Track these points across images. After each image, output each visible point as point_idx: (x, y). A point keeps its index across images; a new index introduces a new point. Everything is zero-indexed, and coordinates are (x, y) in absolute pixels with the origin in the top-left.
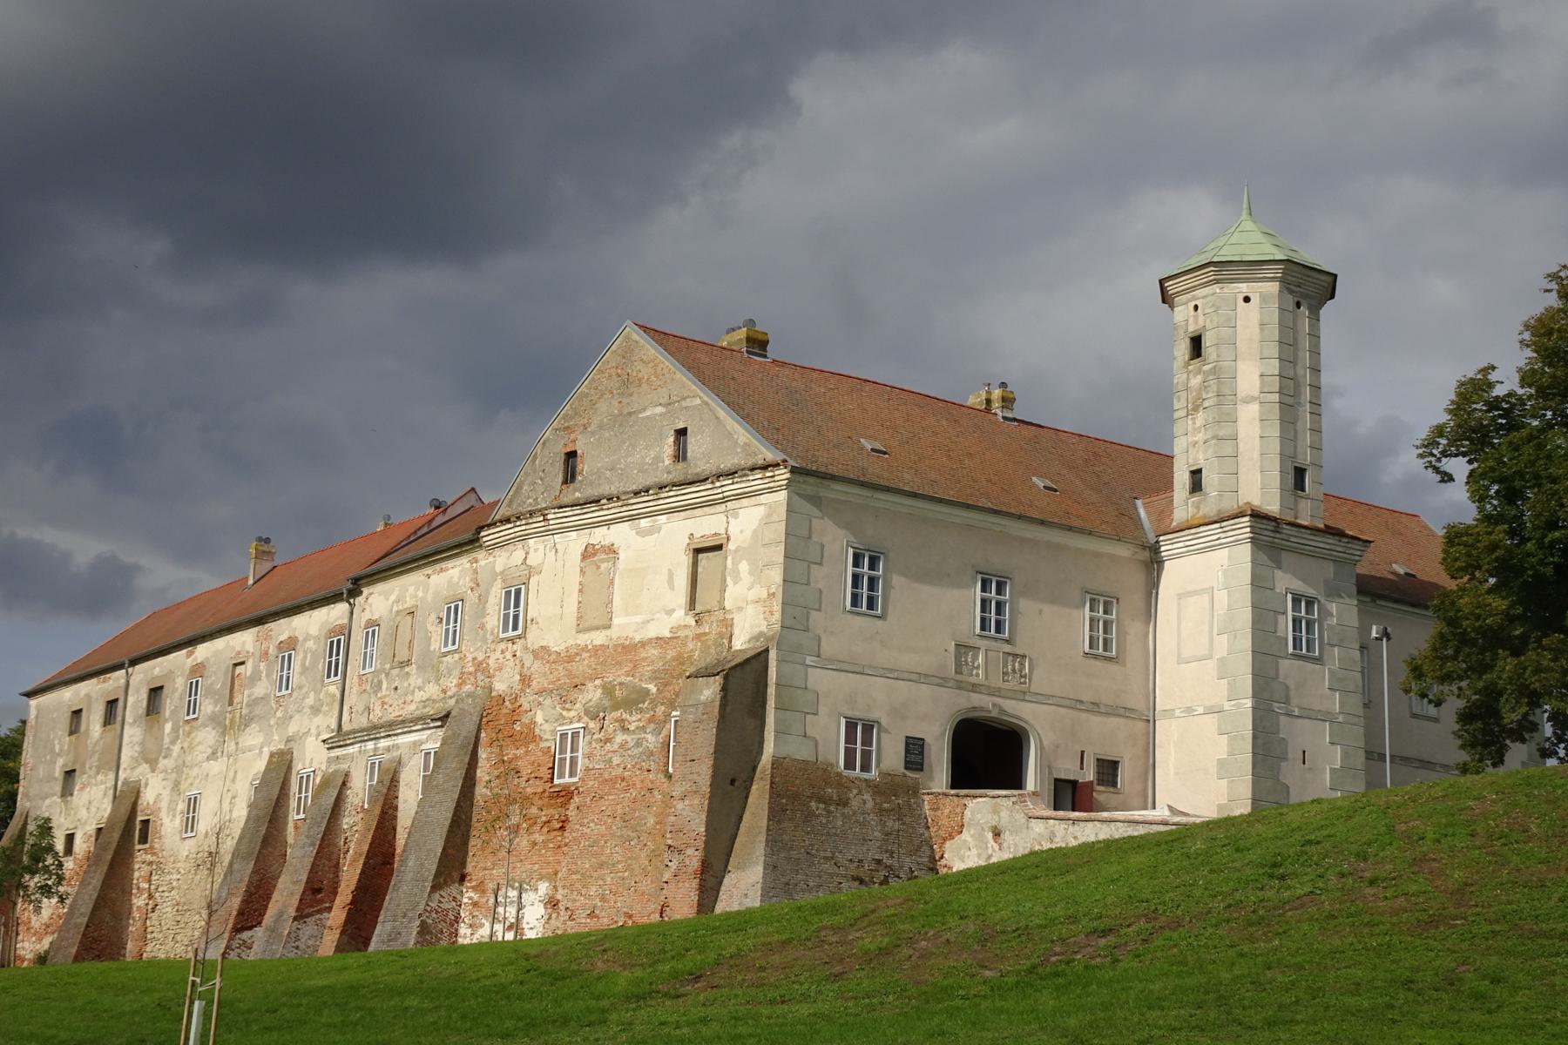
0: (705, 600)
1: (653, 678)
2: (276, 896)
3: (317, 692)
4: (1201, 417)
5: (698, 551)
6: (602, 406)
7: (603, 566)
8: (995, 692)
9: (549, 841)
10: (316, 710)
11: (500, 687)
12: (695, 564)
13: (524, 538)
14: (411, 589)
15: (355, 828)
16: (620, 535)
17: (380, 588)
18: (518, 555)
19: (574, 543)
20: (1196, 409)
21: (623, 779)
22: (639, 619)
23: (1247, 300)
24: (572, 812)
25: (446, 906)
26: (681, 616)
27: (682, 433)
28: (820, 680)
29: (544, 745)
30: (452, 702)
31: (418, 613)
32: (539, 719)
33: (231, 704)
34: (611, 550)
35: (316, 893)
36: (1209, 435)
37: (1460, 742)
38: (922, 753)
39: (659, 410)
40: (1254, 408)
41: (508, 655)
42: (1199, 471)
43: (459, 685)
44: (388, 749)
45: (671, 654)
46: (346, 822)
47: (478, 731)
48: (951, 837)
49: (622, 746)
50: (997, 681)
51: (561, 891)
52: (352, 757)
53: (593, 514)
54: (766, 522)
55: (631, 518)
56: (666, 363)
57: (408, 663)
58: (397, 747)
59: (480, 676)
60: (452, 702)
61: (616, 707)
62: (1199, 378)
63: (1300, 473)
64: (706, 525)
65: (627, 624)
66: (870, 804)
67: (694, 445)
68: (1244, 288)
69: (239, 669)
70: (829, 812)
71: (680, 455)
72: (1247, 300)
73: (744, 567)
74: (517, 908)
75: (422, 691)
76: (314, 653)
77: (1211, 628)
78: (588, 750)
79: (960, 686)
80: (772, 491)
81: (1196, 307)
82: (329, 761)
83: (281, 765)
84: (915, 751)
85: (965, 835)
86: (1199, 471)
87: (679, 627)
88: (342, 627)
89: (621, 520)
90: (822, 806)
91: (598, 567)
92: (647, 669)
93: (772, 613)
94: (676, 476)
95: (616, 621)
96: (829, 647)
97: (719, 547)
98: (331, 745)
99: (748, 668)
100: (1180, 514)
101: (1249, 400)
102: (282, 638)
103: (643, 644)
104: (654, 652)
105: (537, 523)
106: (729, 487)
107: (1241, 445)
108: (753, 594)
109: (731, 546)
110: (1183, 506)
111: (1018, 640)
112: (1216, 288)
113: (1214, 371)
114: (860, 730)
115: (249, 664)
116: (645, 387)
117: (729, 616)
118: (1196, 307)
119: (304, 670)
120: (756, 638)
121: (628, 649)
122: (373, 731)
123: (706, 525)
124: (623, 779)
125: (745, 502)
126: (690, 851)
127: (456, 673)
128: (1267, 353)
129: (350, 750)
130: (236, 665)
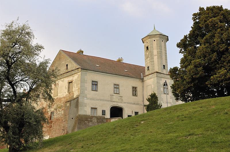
0: (71, 91)
5: (69, 83)
12: (69, 85)
23: (154, 41)
27: (67, 65)
28: (86, 101)
37: (186, 35)
38: (105, 112)
39: (64, 62)
40: (156, 56)
42: (149, 67)
49: (59, 114)
50: (117, 100)
54: (78, 77)
56: (67, 57)
63: (147, 47)
64: (70, 79)
68: (154, 39)
71: (67, 69)
72: (154, 41)
73: (75, 84)
79: (111, 101)
84: (104, 112)
86: (149, 67)
92: (62, 102)
94: (66, 72)
95: (58, 95)
96: (88, 96)
97: (72, 82)
99: (75, 100)
100: (146, 74)
101: (155, 56)
104: (63, 99)
106: (73, 72)
107: (155, 62)
108: (76, 89)
109: (73, 82)
110: (147, 73)
111: (120, 93)
112: (150, 39)
114: (94, 109)
120: (77, 96)
128: (158, 48)
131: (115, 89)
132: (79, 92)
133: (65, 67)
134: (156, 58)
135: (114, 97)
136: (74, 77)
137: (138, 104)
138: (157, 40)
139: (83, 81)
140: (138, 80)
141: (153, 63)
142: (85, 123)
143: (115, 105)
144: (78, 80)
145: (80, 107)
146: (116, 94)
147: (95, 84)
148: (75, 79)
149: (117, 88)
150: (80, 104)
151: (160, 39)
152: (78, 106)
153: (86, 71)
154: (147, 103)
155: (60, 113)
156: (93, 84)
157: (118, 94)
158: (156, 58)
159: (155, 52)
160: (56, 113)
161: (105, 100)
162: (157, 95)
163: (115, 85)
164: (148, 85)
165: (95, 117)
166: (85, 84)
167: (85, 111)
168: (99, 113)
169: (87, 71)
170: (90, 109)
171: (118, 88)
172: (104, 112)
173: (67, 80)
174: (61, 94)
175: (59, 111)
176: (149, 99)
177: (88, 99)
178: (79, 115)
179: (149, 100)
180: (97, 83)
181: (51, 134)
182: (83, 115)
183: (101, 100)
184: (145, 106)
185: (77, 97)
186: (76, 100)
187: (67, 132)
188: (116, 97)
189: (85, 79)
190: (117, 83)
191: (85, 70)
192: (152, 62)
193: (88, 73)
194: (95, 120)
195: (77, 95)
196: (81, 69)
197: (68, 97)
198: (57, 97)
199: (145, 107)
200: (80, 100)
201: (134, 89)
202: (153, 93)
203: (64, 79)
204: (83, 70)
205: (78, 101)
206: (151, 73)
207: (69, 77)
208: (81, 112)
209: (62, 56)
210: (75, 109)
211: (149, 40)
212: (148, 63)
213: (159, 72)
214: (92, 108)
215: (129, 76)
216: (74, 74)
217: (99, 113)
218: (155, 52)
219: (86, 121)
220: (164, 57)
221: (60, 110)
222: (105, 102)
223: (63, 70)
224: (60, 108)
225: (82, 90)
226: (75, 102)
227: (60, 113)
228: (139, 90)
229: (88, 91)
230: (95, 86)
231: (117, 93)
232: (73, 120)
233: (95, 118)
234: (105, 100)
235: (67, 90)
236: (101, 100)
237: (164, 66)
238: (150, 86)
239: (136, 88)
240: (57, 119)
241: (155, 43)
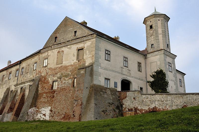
0: (80, 58)
1: (70, 71)
2: (5, 109)
3: (14, 79)
4: (153, 37)
5: (79, 50)
6: (62, 29)
7: (61, 54)
8: (126, 75)
9: (51, 100)
10: (14, 81)
11: (43, 75)
12: (78, 52)
13: (47, 51)
14: (29, 62)
15: (18, 98)
16: (63, 49)
17: (24, 62)
18: (46, 54)
19: (56, 51)
20: (152, 36)
21: (65, 89)
22: (67, 62)
23: (159, 20)
24: (55, 95)
25: (32, 111)
26: (75, 61)
28: (100, 70)
29: (50, 83)
30: (34, 78)
31: (30, 65)
32: (49, 79)
33: (2, 81)
34: (63, 51)
35: (11, 109)
36: (155, 39)
39: (72, 29)
40: (161, 35)
41: (44, 69)
43: (36, 75)
44: (24, 86)
45: (73, 67)
46: (17, 98)
47: (39, 82)
48: (124, 99)
49: (64, 83)
50: (126, 73)
51: (53, 109)
52: (18, 88)
53: (60, 46)
54: (92, 44)
55: (66, 46)
57: (28, 73)
58: (25, 85)
59: (39, 73)
60: (34, 78)
61: (63, 77)
62: (152, 31)
64: (80, 46)
65: (65, 63)
66: (110, 93)
67: (77, 33)
68: (158, 18)
69: (4, 77)
70: (104, 94)
71: (75, 36)
72: (159, 20)
73: (87, 52)
74: (45, 113)
75: (30, 76)
76: (14, 73)
77: (157, 67)
78: (58, 84)
79: (122, 74)
80: (93, 39)
81: (151, 22)
82: (15, 88)
83: (8, 89)
84: (116, 84)
85: (127, 98)
87: (75, 63)
88: (18, 69)
89: (65, 46)
90: (102, 93)
91: (60, 54)
92: (69, 70)
93: (93, 59)
95: (63, 63)
96: (102, 65)
97: (83, 49)
98: (15, 86)
101: (160, 34)
102: (10, 71)
103: (68, 66)
104: (70, 67)
105: (50, 48)
106: (85, 39)
108: (89, 56)
109: (85, 49)
112: (154, 18)
113: (155, 30)
115: (5, 76)
116: (69, 25)
117: (84, 60)
118: (151, 22)
119: (13, 76)
120: (90, 63)
121: (66, 67)
122: (22, 83)
123: (80, 46)
124: (65, 89)
125: (87, 41)
126: (79, 101)
127: (35, 73)
129: (18, 86)
130: (3, 76)
132: (94, 60)
133: (73, 34)
134: (160, 37)
135: (124, 70)
136: (86, 44)
139: (97, 48)
142: (101, 94)
143: (125, 78)
144: (92, 46)
145: (94, 76)
147: (108, 53)
148: (88, 46)
150: (95, 73)
152: (92, 75)
154: (152, 80)
155: (66, 82)
156: (106, 53)
157: (127, 67)
158: (160, 37)
159: (160, 31)
160: (60, 82)
162: (164, 72)
163: (124, 57)
164: (152, 62)
165: (109, 88)
167: (100, 81)
169: (102, 38)
170: (104, 79)
172: (116, 84)
173: (74, 48)
174: (67, 62)
175: (65, 80)
176: (153, 75)
177: (102, 68)
178: (95, 85)
179: (153, 76)
180: (110, 53)
181: (53, 105)
182: (98, 85)
183: (113, 71)
184: (148, 82)
185: (91, 64)
186: (90, 67)
187: (82, 103)
188: (125, 70)
189: (100, 47)
190: (126, 56)
191: (99, 37)
192: (157, 39)
194: (109, 92)
195: (90, 62)
196: (97, 35)
197: (77, 65)
198: (61, 65)
199: (148, 83)
200: (95, 68)
201: (139, 64)
202: (159, 70)
203: (72, 45)
205: (92, 70)
206: (156, 50)
207: (79, 44)
208: (96, 82)
209: (69, 23)
210: (89, 77)
211: (153, 20)
212: (152, 41)
214: (106, 79)
216: (86, 40)
218: (160, 31)
219: (101, 92)
220: (167, 36)
221: (65, 78)
222: (117, 74)
223: (70, 36)
224: (66, 76)
225: (97, 57)
226: (90, 69)
227: (66, 82)
228: (143, 65)
229: (102, 60)
232: (88, 90)
233: (109, 90)
234: (117, 72)
235: (75, 58)
237: (168, 45)
238: (156, 63)
239: (140, 63)
240: (63, 89)
241: (159, 23)
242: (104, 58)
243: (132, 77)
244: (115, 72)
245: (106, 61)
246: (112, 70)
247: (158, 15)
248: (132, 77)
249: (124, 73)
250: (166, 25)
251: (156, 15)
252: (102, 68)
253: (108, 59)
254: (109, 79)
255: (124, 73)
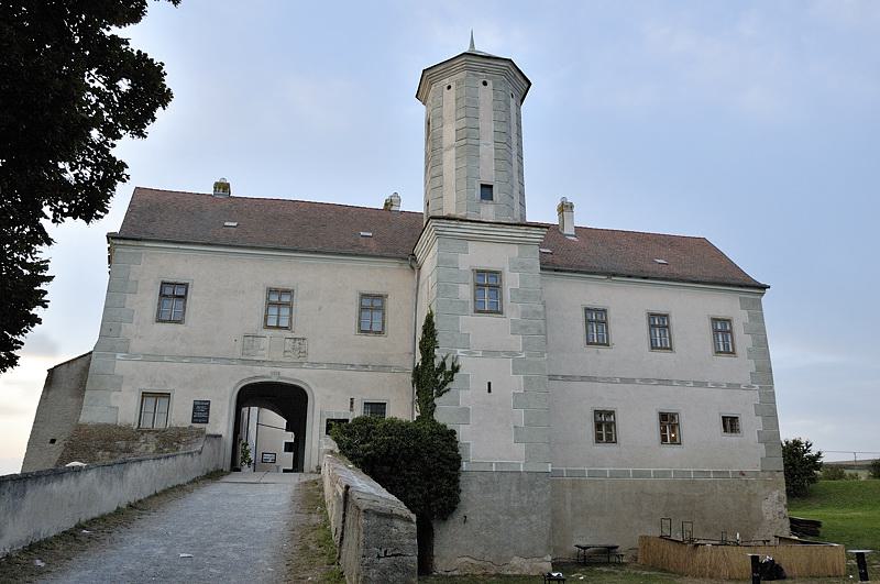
28: (122, 365)
38: (208, 411)
40: (453, 151)
50: (278, 356)
72: (485, 84)
84: (201, 411)
96: (136, 345)
131: (273, 311)
135: (265, 343)
137: (382, 368)
138: (495, 84)
140: (396, 266)
141: (438, 184)
143: (263, 377)
146: (277, 332)
149: (596, 321)
151: (472, 77)
153: (135, 243)
154: (37, 311)
161: (215, 359)
166: (130, 298)
168: (181, 415)
171: (289, 305)
172: (201, 411)
182: (98, 426)
183: (193, 358)
189: (132, 278)
193: (148, 251)
204: (121, 242)
205: (86, 369)
213: (461, 214)
215: (144, 236)
217: (181, 415)
222: (214, 367)
229: (138, 324)
230: (600, 327)
231: (278, 327)
234: (215, 359)
236: (193, 358)
242: (582, 340)
243: (314, 365)
244: (202, 362)
245: (593, 349)
246: (185, 357)
247: (442, 67)
248: (314, 365)
249: (263, 355)
250: (513, 107)
251: (472, 60)
252: (136, 355)
253: (600, 327)
254: (168, 395)
255: (263, 355)
